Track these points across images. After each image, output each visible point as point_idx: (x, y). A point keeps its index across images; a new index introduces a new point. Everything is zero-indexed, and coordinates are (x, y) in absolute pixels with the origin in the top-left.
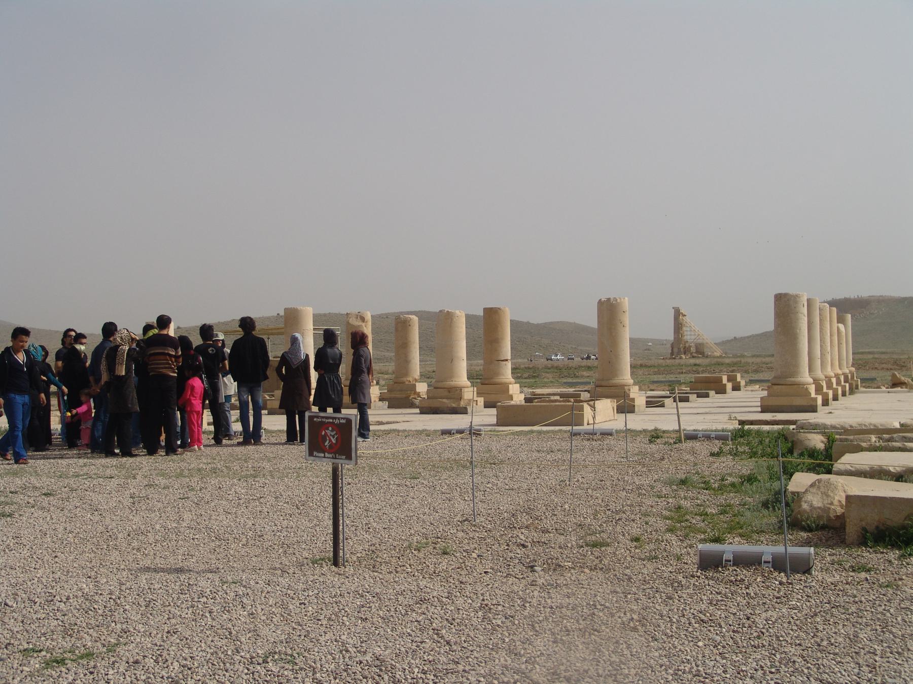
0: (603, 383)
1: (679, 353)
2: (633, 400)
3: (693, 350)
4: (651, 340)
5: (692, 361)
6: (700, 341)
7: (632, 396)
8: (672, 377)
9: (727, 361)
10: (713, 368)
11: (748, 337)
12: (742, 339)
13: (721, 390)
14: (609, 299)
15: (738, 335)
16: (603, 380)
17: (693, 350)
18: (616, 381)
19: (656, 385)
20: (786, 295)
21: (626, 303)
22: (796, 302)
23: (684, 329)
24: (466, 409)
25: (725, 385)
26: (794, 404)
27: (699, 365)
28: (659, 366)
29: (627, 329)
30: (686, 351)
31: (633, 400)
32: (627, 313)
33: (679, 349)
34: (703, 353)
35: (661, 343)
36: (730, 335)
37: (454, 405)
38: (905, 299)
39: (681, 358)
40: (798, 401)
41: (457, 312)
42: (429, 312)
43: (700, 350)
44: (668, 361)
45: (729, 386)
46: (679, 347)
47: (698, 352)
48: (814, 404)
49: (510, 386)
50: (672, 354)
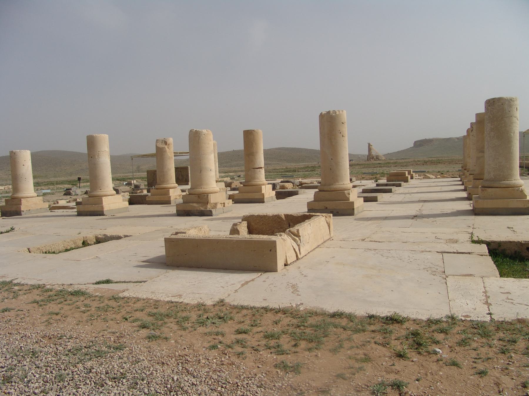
0: (326, 188)
1: (370, 159)
2: (353, 203)
3: (375, 158)
7: (351, 200)
12: (391, 153)
13: (406, 181)
14: (329, 112)
17: (375, 158)
20: (500, 99)
21: (345, 116)
22: (510, 106)
24: (211, 211)
28: (364, 164)
29: (346, 138)
30: (373, 158)
31: (353, 203)
32: (346, 125)
37: (202, 209)
41: (204, 131)
43: (377, 158)
45: (409, 177)
46: (370, 157)
49: (263, 187)
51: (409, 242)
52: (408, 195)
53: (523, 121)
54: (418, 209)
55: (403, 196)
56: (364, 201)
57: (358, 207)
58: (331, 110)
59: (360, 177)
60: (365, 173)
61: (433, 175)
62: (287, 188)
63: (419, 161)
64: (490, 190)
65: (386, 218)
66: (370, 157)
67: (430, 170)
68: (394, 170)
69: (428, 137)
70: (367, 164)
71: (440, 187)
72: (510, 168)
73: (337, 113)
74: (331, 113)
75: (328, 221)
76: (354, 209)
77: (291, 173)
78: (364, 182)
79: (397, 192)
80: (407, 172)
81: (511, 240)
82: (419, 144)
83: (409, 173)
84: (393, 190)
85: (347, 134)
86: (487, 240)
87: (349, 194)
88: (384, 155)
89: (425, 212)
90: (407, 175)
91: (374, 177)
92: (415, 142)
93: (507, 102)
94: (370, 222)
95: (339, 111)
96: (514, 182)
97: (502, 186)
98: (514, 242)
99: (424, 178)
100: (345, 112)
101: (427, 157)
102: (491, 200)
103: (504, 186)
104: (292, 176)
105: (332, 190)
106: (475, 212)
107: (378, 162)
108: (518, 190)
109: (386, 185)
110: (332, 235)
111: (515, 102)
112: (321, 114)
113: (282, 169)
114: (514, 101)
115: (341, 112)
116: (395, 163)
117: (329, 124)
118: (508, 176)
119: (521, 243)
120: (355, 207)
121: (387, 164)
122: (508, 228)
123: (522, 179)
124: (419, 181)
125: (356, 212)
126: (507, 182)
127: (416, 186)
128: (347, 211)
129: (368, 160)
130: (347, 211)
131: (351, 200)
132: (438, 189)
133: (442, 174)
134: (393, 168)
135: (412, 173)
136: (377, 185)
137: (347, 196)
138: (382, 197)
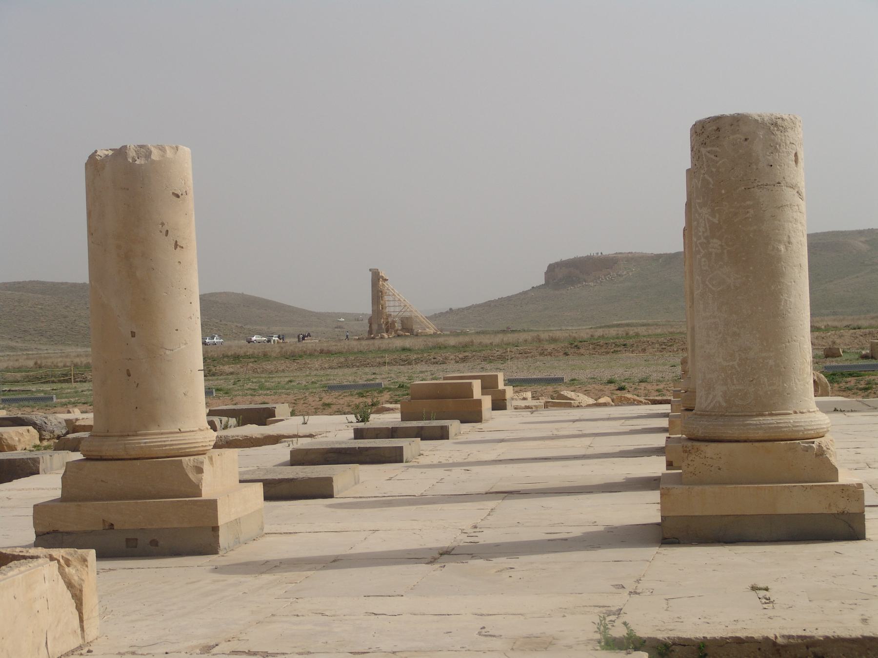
0: (109, 448)
1: (380, 330)
2: (212, 505)
3: (398, 326)
4: (344, 315)
5: (399, 343)
6: (407, 314)
8: (363, 376)
9: (452, 341)
10: (432, 355)
11: (468, 308)
13: (472, 415)
14: (121, 153)
15: (454, 307)
16: (106, 436)
17: (398, 326)
18: (154, 439)
19: (335, 393)
20: (737, 121)
21: (185, 166)
22: (774, 147)
23: (386, 298)
25: (479, 402)
26: (784, 509)
27: (409, 350)
28: (350, 352)
29: (191, 255)
30: (389, 327)
31: (212, 505)
32: (190, 203)
33: (380, 325)
34: (411, 331)
35: (357, 318)
36: (443, 306)
38: (659, 257)
39: (382, 338)
40: (796, 501)
42: (43, 283)
43: (407, 327)
44: (364, 343)
45: (487, 402)
46: (380, 323)
47: (403, 329)
48: (853, 509)
50: (370, 332)
51: (379, 650)
52: (457, 472)
53: (816, 200)
54: (467, 525)
55: (440, 473)
56: (268, 497)
57: (237, 521)
58: (132, 144)
59: (314, 401)
60: (332, 388)
61: (587, 393)
62: (13, 448)
63: (554, 340)
64: (710, 449)
65: (335, 562)
66: (380, 323)
67: (582, 376)
68: (425, 376)
69: (608, 249)
70: (258, 360)
71: (587, 441)
72: (780, 371)
73: (156, 155)
74: (132, 153)
75: (75, 579)
76: (216, 529)
77: (47, 387)
78: (318, 422)
79: (423, 461)
80: (477, 385)
81: (742, 634)
82: (566, 275)
83: (489, 385)
84: (406, 454)
85: (194, 236)
86: (661, 636)
87: (199, 470)
88: (434, 318)
89: (487, 537)
90: (477, 393)
91: (363, 400)
92: (552, 268)
93: (761, 133)
94: (267, 578)
95: (162, 149)
96: (793, 419)
97: (752, 435)
98: (750, 640)
99: (547, 405)
100: (186, 151)
101: (570, 328)
102: (716, 488)
103: (760, 435)
104: (45, 401)
105: (133, 454)
106: (671, 533)
107: (408, 343)
108: (806, 449)
109: (393, 433)
110: (92, 631)
111: (790, 133)
112: (92, 157)
113: (19, 369)
114: (784, 130)
115: (169, 153)
116: (465, 347)
117: (124, 198)
118: (774, 398)
119: (774, 644)
120: (222, 520)
121: (435, 353)
122: (754, 588)
123: (824, 408)
124: (527, 416)
125: (224, 538)
126: (769, 420)
127: (513, 435)
128: (193, 535)
129: (371, 334)
130: (193, 535)
131: (207, 493)
132: (578, 446)
133: (619, 391)
134: (452, 365)
135: (501, 386)
136: (359, 434)
137: (192, 476)
138: (370, 478)
